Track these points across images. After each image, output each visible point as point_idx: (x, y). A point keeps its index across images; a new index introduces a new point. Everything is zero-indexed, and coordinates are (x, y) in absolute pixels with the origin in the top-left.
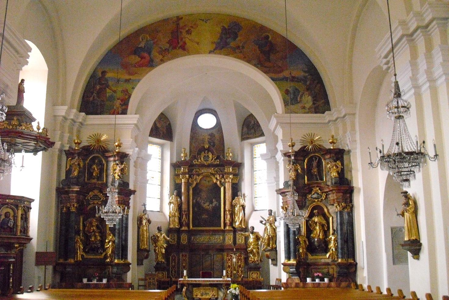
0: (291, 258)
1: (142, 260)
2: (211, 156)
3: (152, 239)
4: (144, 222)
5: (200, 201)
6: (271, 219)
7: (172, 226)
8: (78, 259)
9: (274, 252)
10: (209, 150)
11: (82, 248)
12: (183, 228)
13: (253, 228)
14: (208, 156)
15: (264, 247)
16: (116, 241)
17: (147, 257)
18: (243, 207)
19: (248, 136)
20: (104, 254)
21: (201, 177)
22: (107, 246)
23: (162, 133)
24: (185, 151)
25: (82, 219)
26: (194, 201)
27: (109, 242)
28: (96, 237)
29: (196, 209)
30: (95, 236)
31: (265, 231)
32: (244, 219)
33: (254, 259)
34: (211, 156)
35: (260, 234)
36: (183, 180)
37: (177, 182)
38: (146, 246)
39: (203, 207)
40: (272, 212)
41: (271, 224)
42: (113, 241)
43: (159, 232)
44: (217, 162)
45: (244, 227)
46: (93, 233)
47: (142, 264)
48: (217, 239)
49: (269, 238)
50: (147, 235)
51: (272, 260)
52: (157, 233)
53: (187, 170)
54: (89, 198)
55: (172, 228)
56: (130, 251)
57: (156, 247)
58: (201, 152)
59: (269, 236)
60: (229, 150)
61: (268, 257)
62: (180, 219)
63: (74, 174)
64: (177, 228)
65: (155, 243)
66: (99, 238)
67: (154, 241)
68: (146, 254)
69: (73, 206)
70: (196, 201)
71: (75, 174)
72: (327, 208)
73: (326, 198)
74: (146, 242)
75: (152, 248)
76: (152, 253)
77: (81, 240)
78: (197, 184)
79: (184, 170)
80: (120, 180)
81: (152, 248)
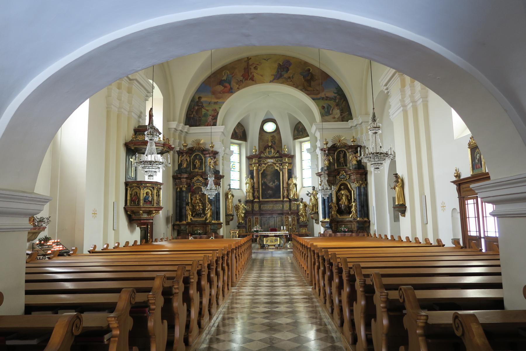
0: (327, 217)
2: (273, 151)
4: (230, 196)
5: (267, 181)
6: (314, 193)
7: (248, 199)
9: (316, 215)
10: (271, 147)
12: (256, 200)
13: (302, 199)
14: (271, 151)
15: (309, 211)
17: (232, 220)
18: (296, 185)
19: (298, 137)
21: (267, 165)
23: (239, 136)
24: (255, 148)
26: (263, 182)
27: (208, 210)
29: (264, 187)
31: (310, 201)
32: (297, 194)
33: (303, 220)
34: (273, 151)
35: (307, 203)
36: (254, 168)
37: (250, 169)
39: (268, 186)
40: (315, 188)
41: (314, 196)
43: (239, 203)
44: (277, 155)
45: (296, 198)
47: (229, 224)
48: (278, 207)
49: (313, 205)
51: (315, 220)
53: (257, 161)
55: (248, 200)
58: (266, 149)
59: (313, 204)
60: (285, 147)
61: (313, 218)
62: (253, 194)
64: (252, 200)
65: (237, 210)
66: (201, 207)
68: (231, 217)
70: (264, 181)
72: (350, 185)
73: (349, 178)
74: (231, 210)
75: (235, 213)
76: (235, 217)
77: (190, 209)
78: (264, 170)
79: (255, 161)
81: (235, 213)
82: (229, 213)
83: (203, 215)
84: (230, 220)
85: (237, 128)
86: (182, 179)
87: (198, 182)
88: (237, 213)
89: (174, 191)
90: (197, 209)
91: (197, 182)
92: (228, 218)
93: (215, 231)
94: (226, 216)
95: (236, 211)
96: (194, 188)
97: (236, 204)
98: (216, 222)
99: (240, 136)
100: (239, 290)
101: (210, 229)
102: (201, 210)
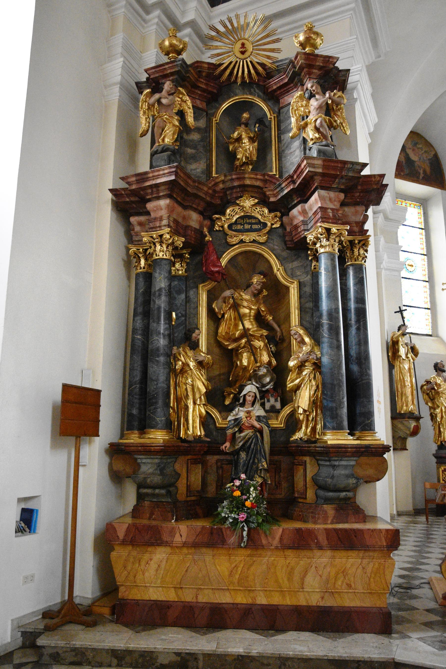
1: (404, 440)
3: (423, 392)
4: (402, 351)
8: (190, 432)
11: (204, 390)
16: (325, 360)
17: (415, 432)
20: (287, 410)
22: (292, 382)
23: (421, 172)
25: (203, 298)
27: (301, 367)
28: (254, 354)
30: (253, 351)
38: (411, 407)
42: (315, 364)
43: (438, 375)
46: (244, 341)
47: (404, 448)
50: (411, 381)
52: (434, 377)
54: (226, 226)
56: (379, 402)
57: (435, 409)
63: (163, 140)
65: (432, 400)
66: (265, 358)
67: (428, 394)
68: (413, 424)
69: (161, 243)
71: (167, 140)
74: (410, 398)
75: (425, 412)
76: (426, 422)
77: (200, 364)
80: (324, 143)
82: (405, 408)
83: (272, 400)
84: (408, 432)
85: (413, 150)
86: (149, 200)
87: (247, 227)
88: (430, 408)
89: (129, 286)
90: (245, 369)
91: (239, 227)
92: (400, 426)
93: (343, 494)
94: (393, 418)
95: (427, 404)
96: (224, 261)
97: (428, 378)
98: (350, 441)
99: (425, 171)
100: (418, 561)
101: (314, 480)
102: (263, 371)
